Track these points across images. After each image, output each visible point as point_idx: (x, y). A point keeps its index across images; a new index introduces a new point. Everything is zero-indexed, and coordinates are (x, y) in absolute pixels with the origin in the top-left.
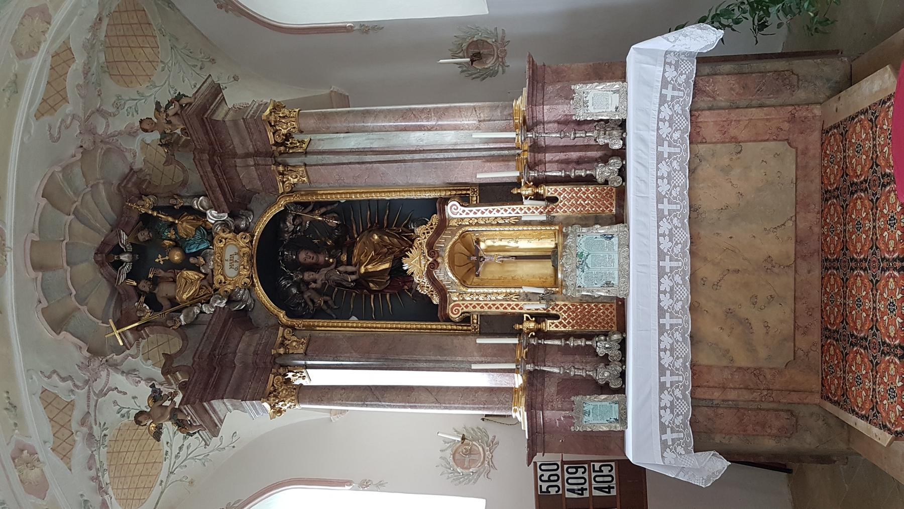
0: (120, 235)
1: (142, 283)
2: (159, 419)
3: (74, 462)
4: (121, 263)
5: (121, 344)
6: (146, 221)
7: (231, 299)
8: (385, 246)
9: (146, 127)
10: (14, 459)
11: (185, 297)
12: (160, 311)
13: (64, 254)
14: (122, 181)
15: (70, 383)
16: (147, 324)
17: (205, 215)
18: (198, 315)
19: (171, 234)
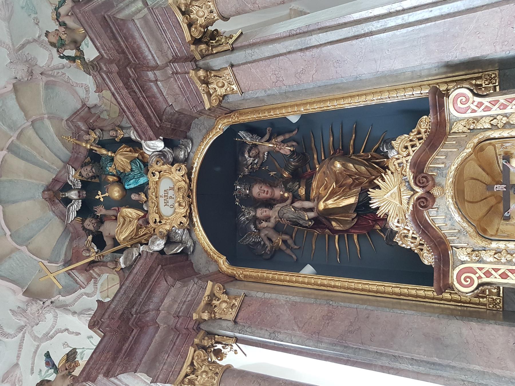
7: (170, 240)
8: (350, 176)
17: (140, 146)
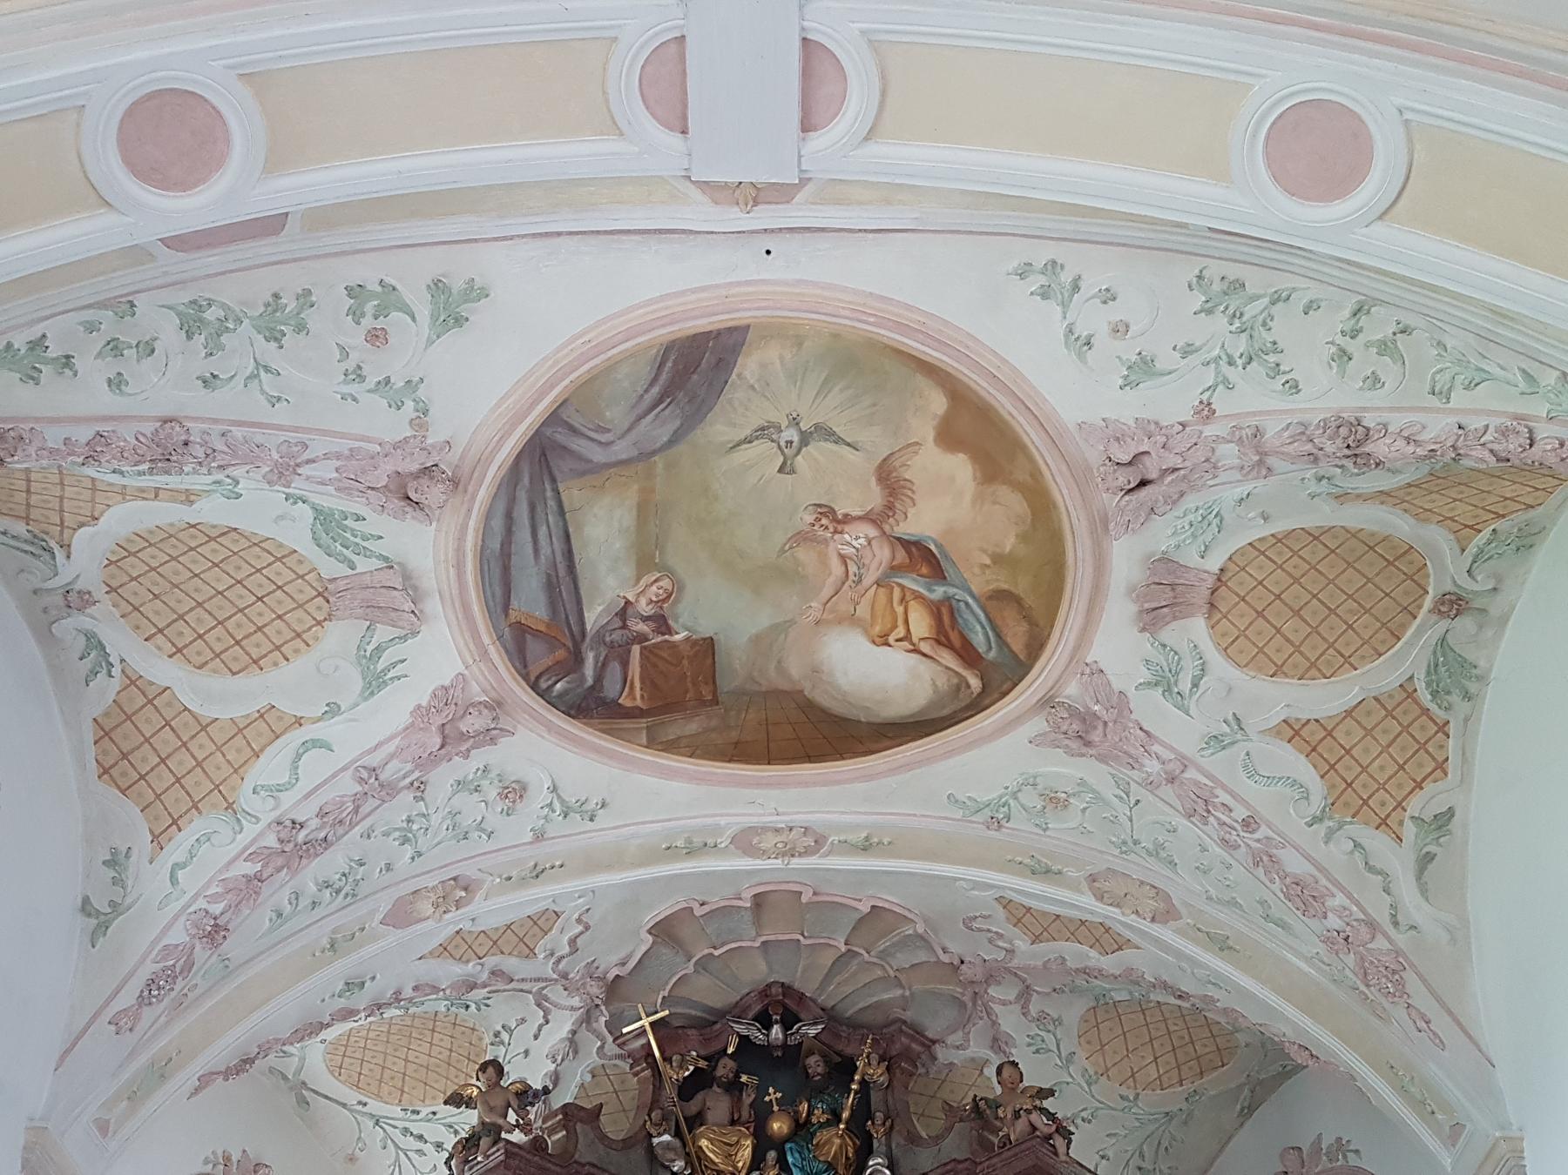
0: (815, 1024)
1: (731, 1064)
2: (486, 1103)
3: (433, 963)
4: (767, 1026)
5: (625, 1030)
6: (843, 1069)
9: (1006, 1072)
10: (454, 879)
11: (704, 1143)
12: (679, 1095)
13: (781, 937)
14: (911, 1027)
15: (567, 949)
16: (657, 1074)
18: (667, 1168)
19: (820, 1116)
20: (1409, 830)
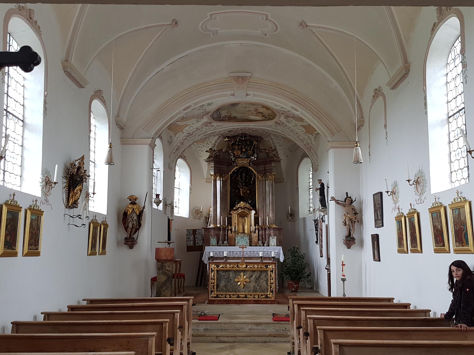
6: (251, 143)
7: (234, 162)
19: (248, 149)
20: (314, 135)
